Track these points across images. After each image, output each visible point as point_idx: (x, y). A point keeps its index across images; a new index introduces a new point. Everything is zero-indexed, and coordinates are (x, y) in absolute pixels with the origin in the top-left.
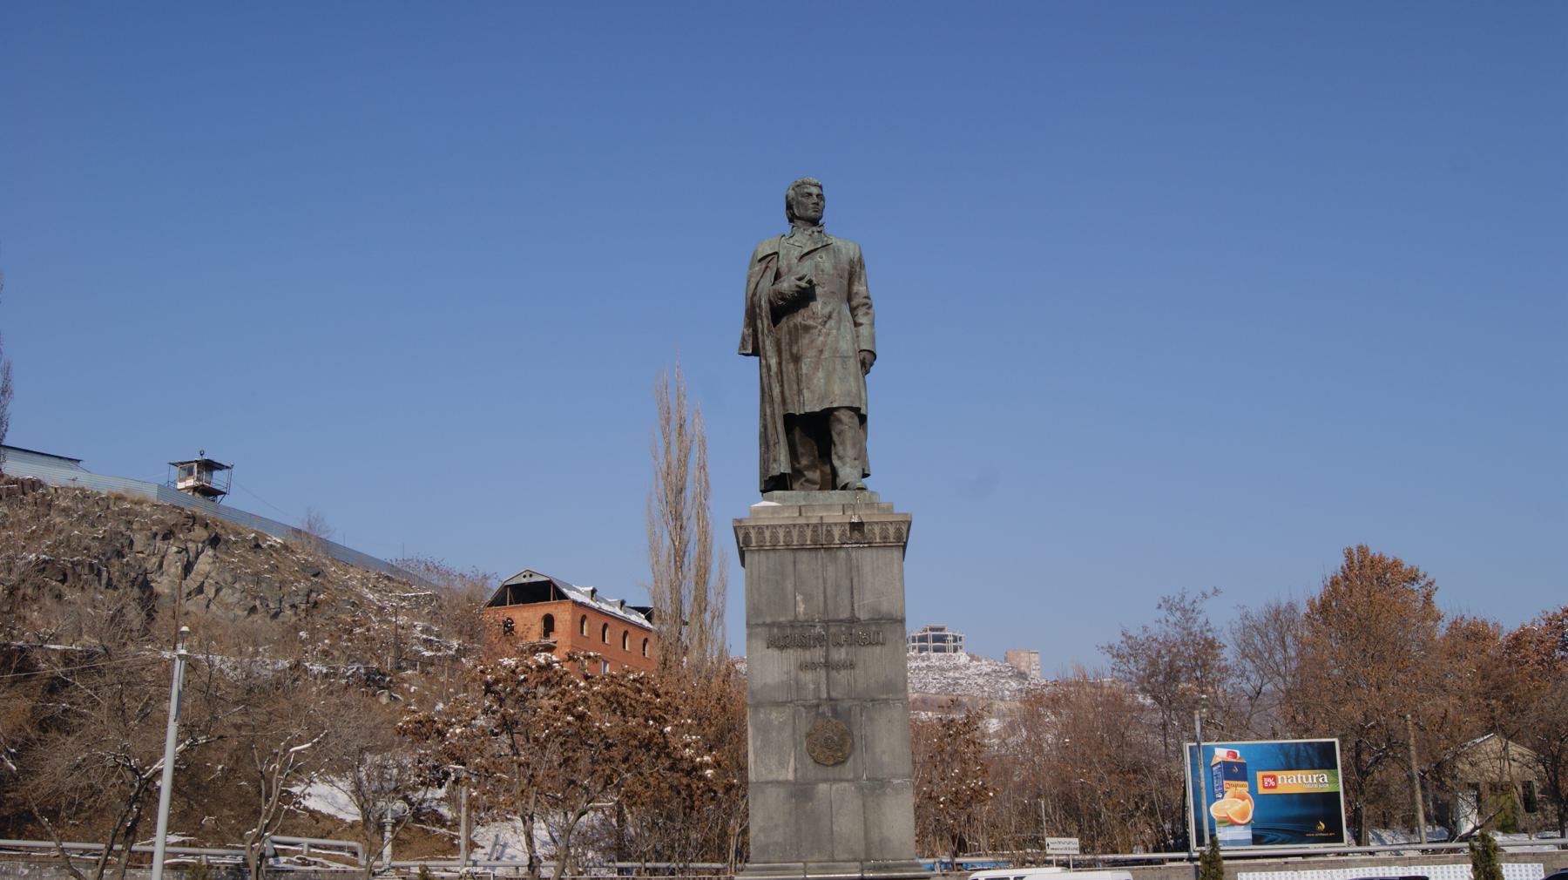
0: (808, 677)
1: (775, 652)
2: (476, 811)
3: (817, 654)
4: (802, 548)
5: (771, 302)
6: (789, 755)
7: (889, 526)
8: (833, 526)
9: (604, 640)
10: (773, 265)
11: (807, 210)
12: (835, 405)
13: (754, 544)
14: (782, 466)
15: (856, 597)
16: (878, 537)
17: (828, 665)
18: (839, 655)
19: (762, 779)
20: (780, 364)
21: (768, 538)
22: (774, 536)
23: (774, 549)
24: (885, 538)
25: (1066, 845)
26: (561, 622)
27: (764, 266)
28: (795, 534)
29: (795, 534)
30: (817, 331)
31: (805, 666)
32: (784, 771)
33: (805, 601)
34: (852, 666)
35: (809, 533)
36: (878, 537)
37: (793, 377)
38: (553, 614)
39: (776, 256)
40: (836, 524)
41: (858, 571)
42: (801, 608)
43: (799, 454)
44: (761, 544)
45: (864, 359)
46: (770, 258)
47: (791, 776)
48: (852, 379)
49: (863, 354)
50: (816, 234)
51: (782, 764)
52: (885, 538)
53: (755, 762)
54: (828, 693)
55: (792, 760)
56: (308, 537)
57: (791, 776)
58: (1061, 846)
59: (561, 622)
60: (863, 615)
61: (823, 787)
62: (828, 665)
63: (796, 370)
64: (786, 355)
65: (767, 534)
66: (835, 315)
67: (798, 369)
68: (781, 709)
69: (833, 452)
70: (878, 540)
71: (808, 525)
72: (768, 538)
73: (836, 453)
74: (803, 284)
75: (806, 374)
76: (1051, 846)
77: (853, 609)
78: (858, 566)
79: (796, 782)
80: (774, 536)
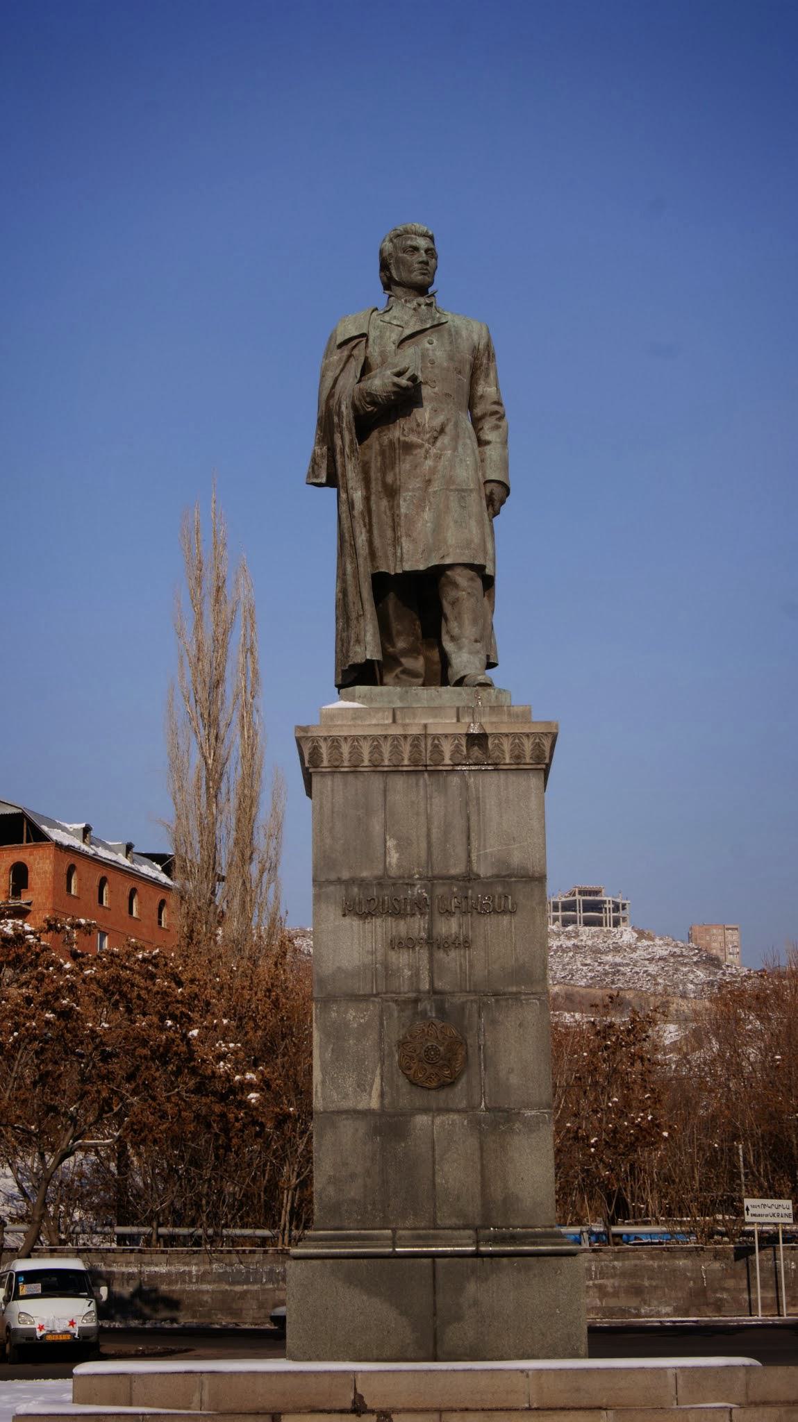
3: (416, 926)
4: (396, 771)
5: (354, 407)
7: (525, 740)
9: (101, 901)
10: (359, 353)
11: (411, 272)
12: (448, 561)
13: (325, 763)
14: (369, 649)
17: (432, 942)
18: (449, 927)
20: (367, 499)
21: (346, 755)
22: (356, 752)
23: (355, 771)
25: (774, 1210)
26: (38, 874)
27: (346, 353)
28: (386, 749)
29: (386, 749)
30: (421, 452)
31: (397, 944)
34: (466, 944)
35: (406, 749)
37: (387, 520)
38: (27, 864)
42: (394, 857)
43: (394, 632)
46: (356, 341)
47: (375, 1104)
48: (473, 523)
51: (362, 1086)
53: (323, 1082)
54: (432, 982)
55: (378, 1080)
57: (375, 1104)
58: (767, 1211)
59: (38, 874)
61: (422, 1120)
62: (432, 942)
63: (392, 508)
64: (376, 486)
65: (345, 749)
66: (449, 428)
67: (393, 507)
69: (444, 631)
71: (405, 737)
72: (346, 755)
73: (448, 632)
74: (403, 381)
76: (752, 1211)
78: (478, 798)
79: (382, 1113)
80: (356, 752)
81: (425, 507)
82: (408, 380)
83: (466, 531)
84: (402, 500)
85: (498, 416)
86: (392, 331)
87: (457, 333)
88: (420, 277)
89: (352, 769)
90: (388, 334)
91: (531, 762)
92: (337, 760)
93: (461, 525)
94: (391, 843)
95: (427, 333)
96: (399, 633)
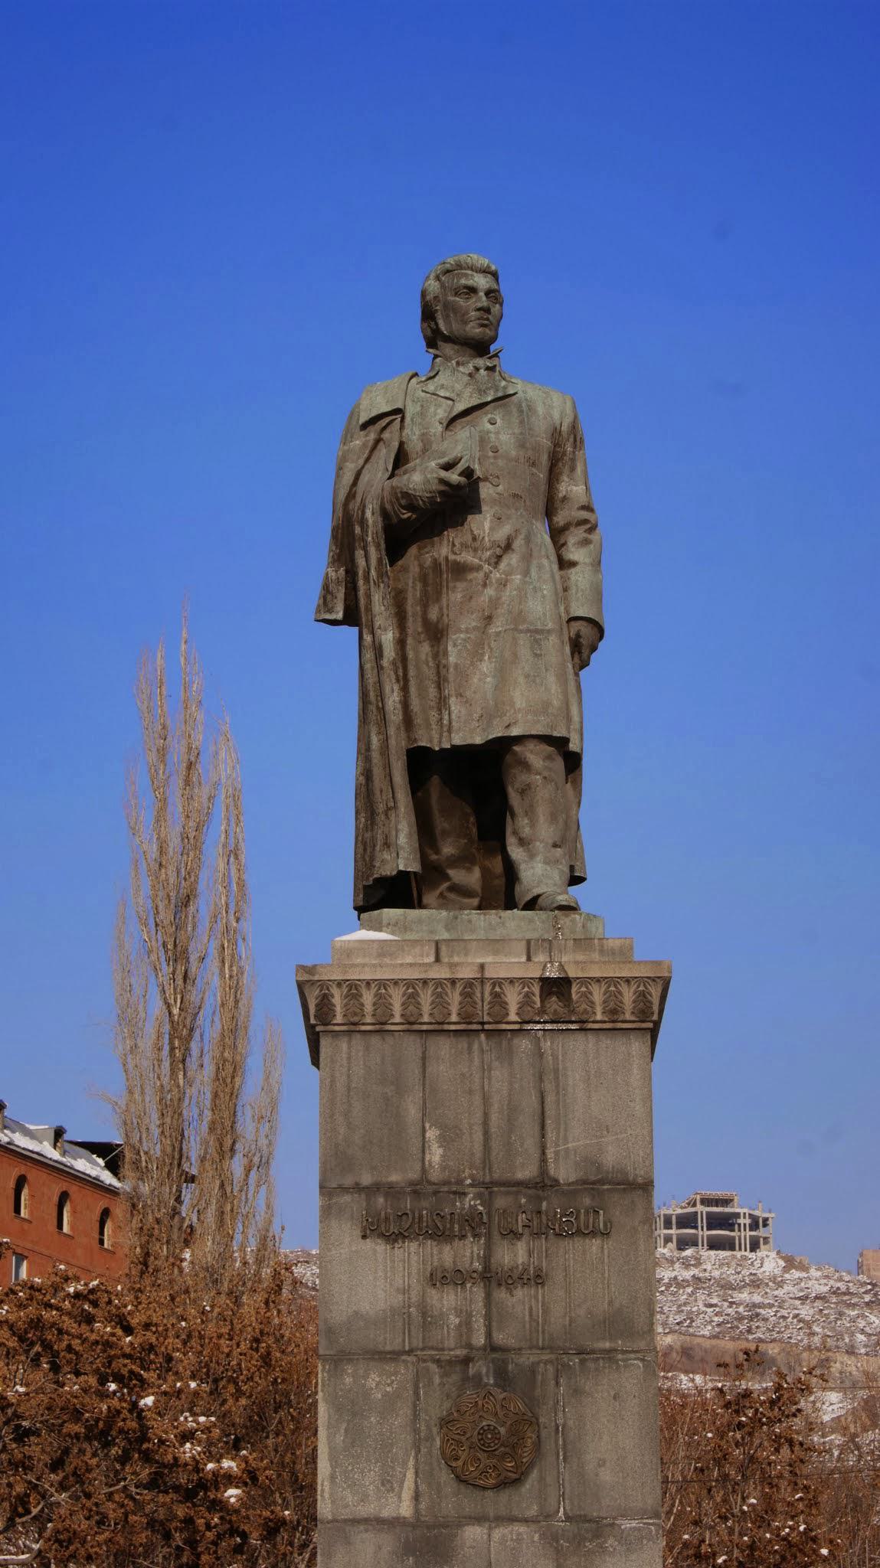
0: (446, 1300)
1: (380, 1247)
3: (467, 1252)
5: (384, 514)
6: (405, 1463)
11: (466, 323)
15: (551, 1135)
16: (599, 1010)
18: (514, 1255)
19: (345, 1514)
31: (439, 1278)
32: (392, 1498)
33: (444, 1140)
36: (599, 1010)
42: (436, 1155)
43: (438, 831)
45: (578, 636)
51: (388, 1484)
53: (333, 1477)
54: (489, 1335)
55: (410, 1475)
60: (564, 1172)
61: (473, 1533)
68: (390, 1367)
75: (456, 666)
77: (543, 1159)
78: (556, 1071)
81: (483, 655)
89: (377, 1027)
91: (633, 1018)
92: (355, 1014)
94: (432, 1134)
96: (445, 833)
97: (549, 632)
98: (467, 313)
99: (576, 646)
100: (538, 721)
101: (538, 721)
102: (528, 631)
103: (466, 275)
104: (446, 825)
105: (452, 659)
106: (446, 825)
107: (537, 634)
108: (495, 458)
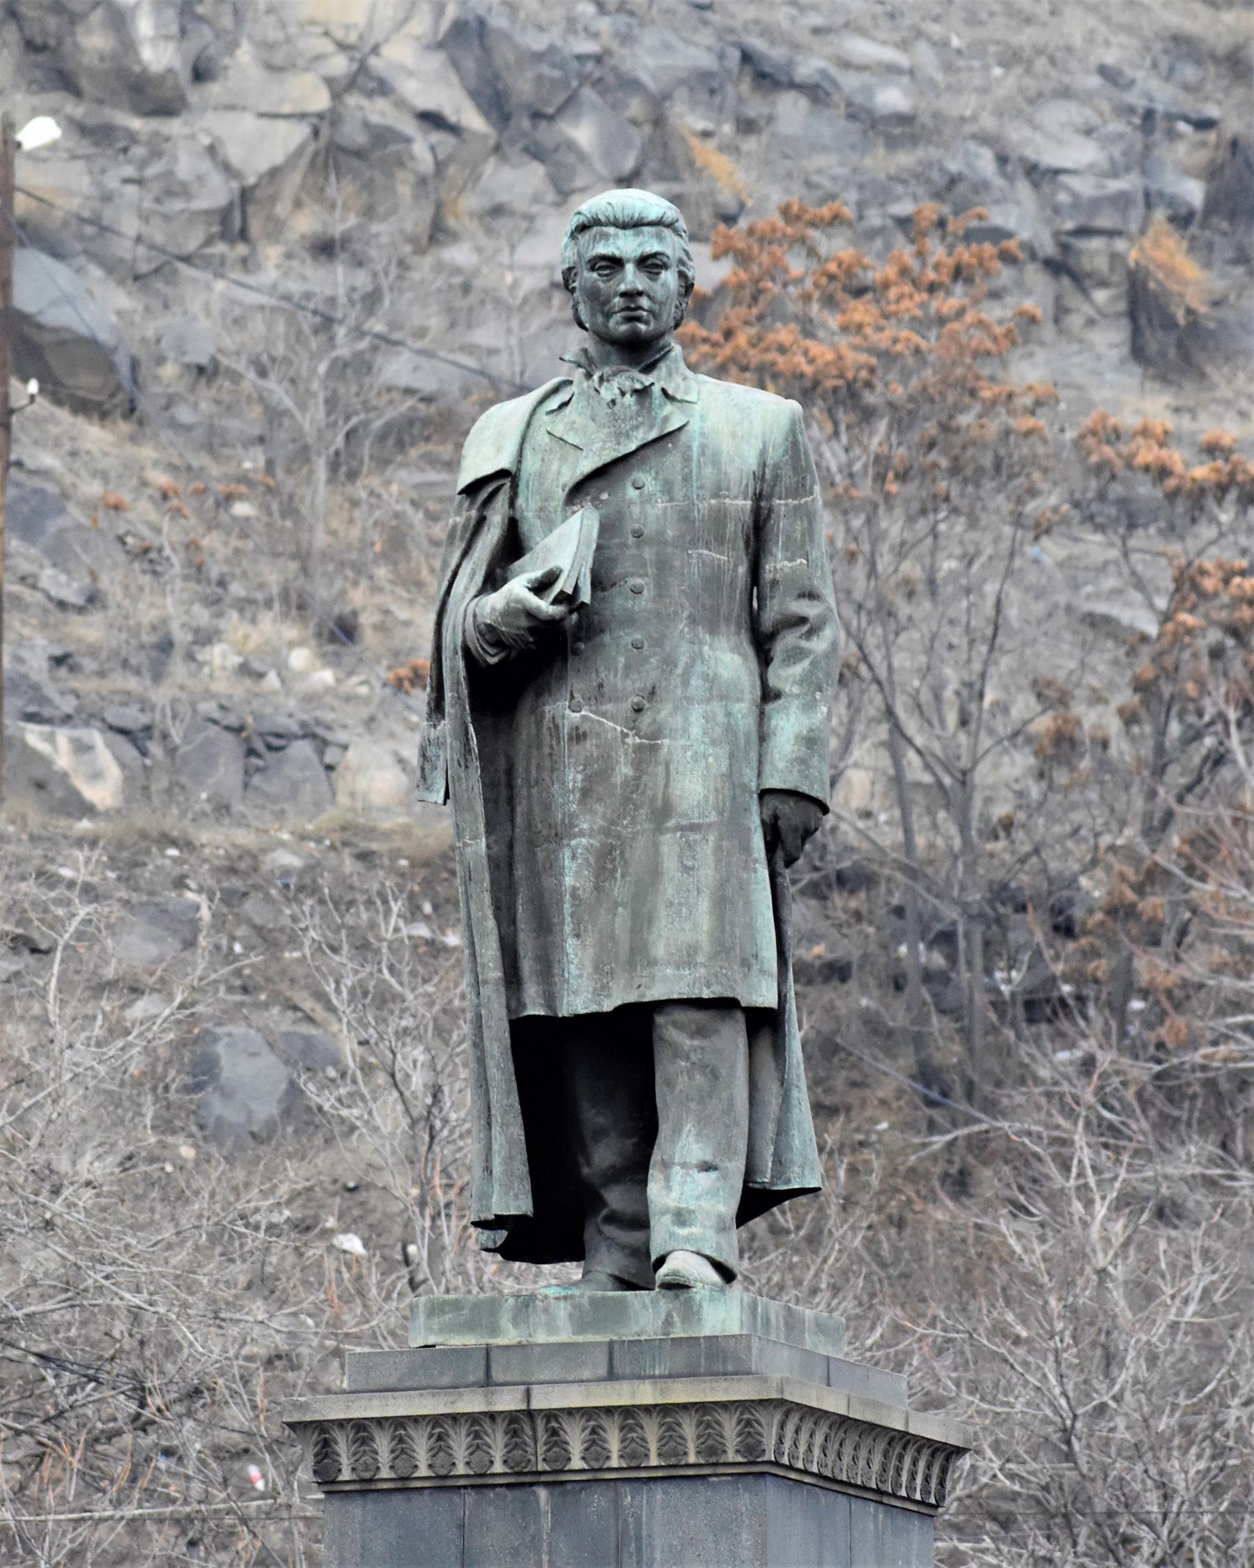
2: (119, 879)
5: (467, 652)
8: (373, 1426)
11: (608, 316)
16: (691, 1447)
24: (633, 1456)
36: (691, 1447)
39: (507, 483)
40: (570, 1412)
41: (639, 1549)
43: (588, 1133)
44: (367, 1475)
45: (776, 818)
46: (490, 488)
48: (704, 906)
49: (773, 802)
50: (629, 399)
52: (712, 1450)
56: (1165, 1497)
70: (692, 1459)
74: (545, 606)
75: (574, 889)
78: (639, 1538)
81: (614, 871)
82: (556, 601)
83: (688, 926)
84: (567, 853)
85: (805, 628)
86: (563, 460)
87: (232, 871)
88: (624, 328)
89: (399, 1485)
90: (555, 467)
91: (740, 1459)
92: (367, 1469)
93: (679, 913)
95: (633, 461)
96: (600, 1133)
97: (709, 826)
98: (608, 301)
99: (773, 839)
100: (681, 978)
101: (681, 978)
102: (682, 829)
103: (605, 237)
104: (601, 1120)
105: (569, 880)
106: (601, 1120)
107: (163, 1145)
108: (638, 545)
